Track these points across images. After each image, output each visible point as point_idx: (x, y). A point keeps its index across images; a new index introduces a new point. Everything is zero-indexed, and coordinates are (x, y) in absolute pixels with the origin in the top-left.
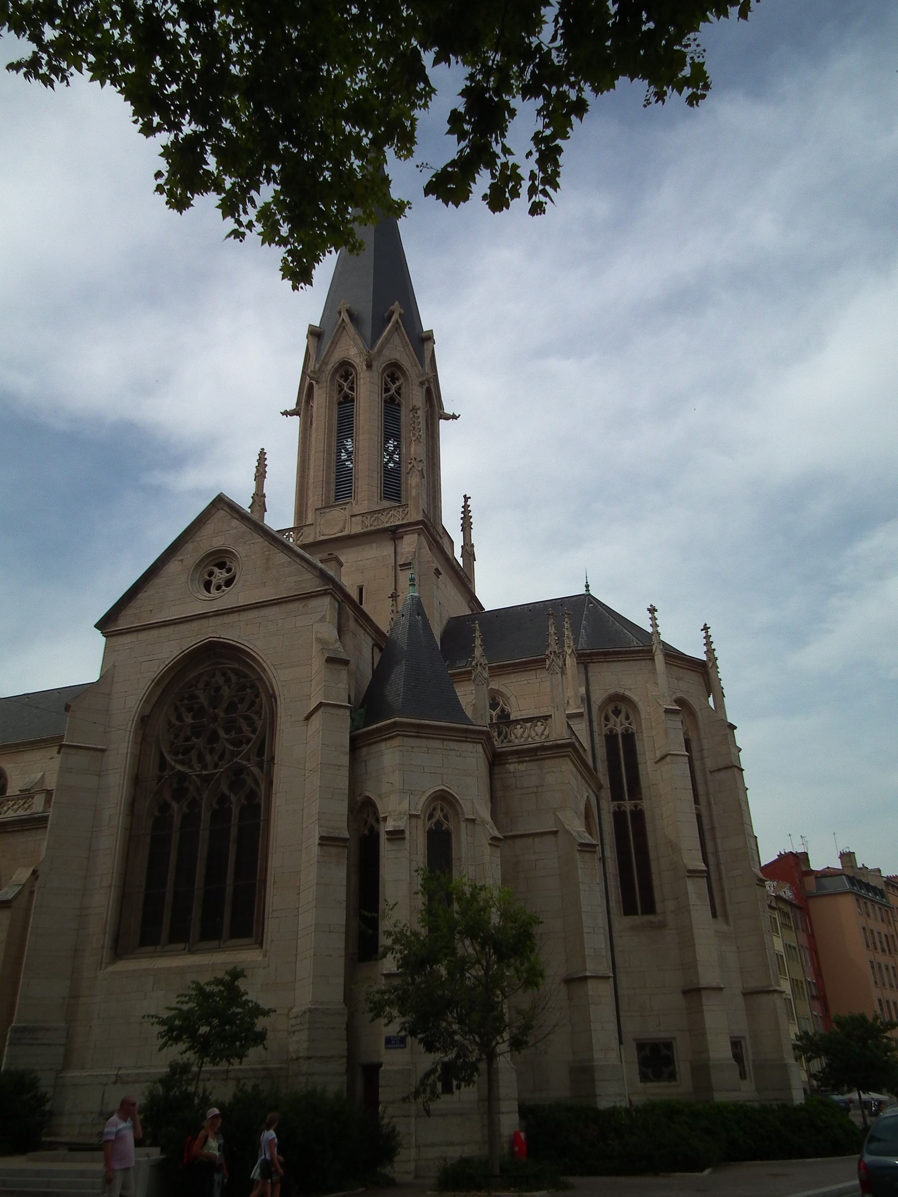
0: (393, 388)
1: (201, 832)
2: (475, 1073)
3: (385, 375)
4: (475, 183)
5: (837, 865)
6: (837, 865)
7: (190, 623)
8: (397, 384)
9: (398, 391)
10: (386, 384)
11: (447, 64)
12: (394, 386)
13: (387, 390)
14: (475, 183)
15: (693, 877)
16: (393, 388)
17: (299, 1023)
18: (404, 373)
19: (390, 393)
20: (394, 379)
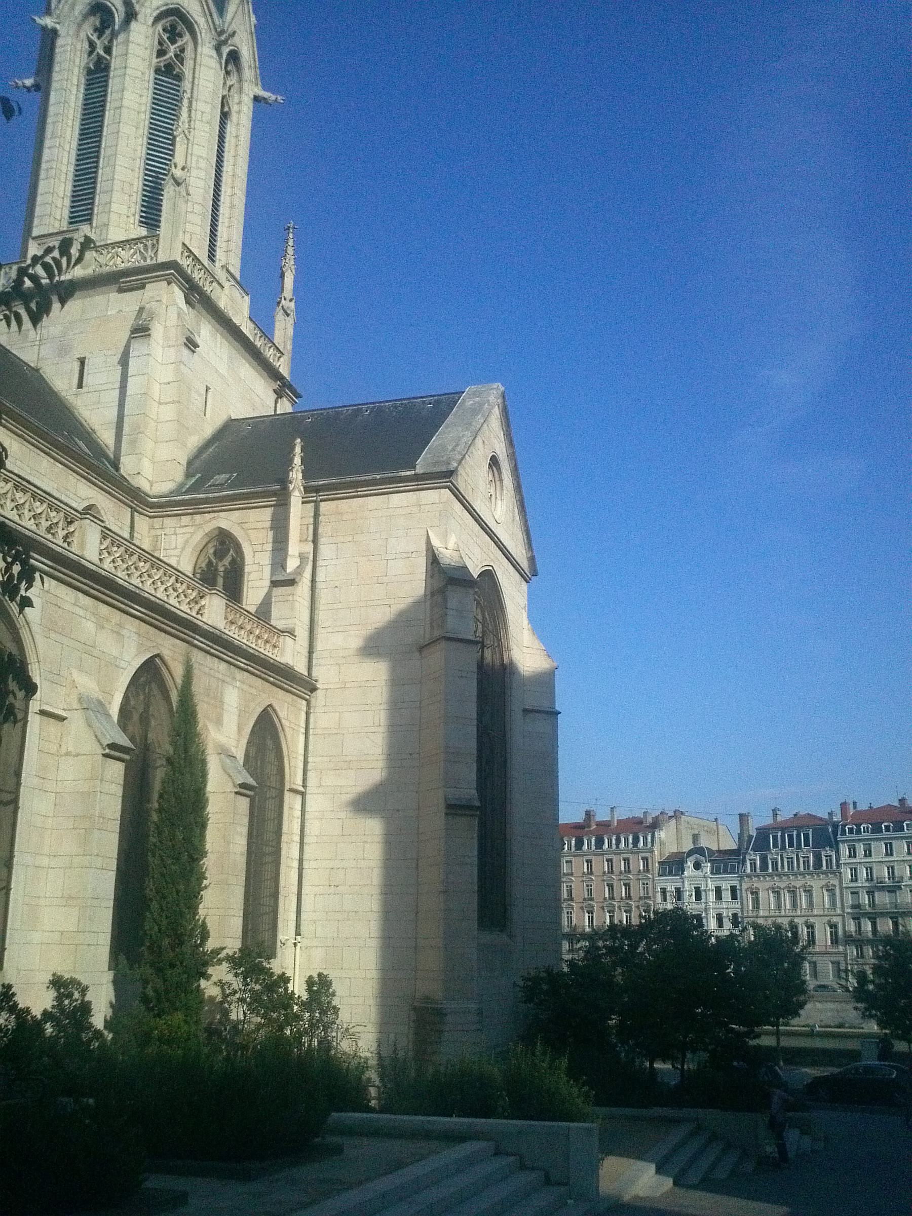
0: (172, 49)
1: (273, 598)
2: (873, 1027)
3: (159, 27)
4: (47, 316)
5: (896, 804)
6: (896, 804)
7: (307, 664)
8: (179, 43)
9: (180, 57)
10: (160, 43)
11: (38, 712)
12: (172, 48)
13: (161, 53)
14: (47, 316)
15: (156, 281)
16: (172, 49)
17: (62, 200)
18: (190, 27)
19: (165, 58)
20: (173, 34)
